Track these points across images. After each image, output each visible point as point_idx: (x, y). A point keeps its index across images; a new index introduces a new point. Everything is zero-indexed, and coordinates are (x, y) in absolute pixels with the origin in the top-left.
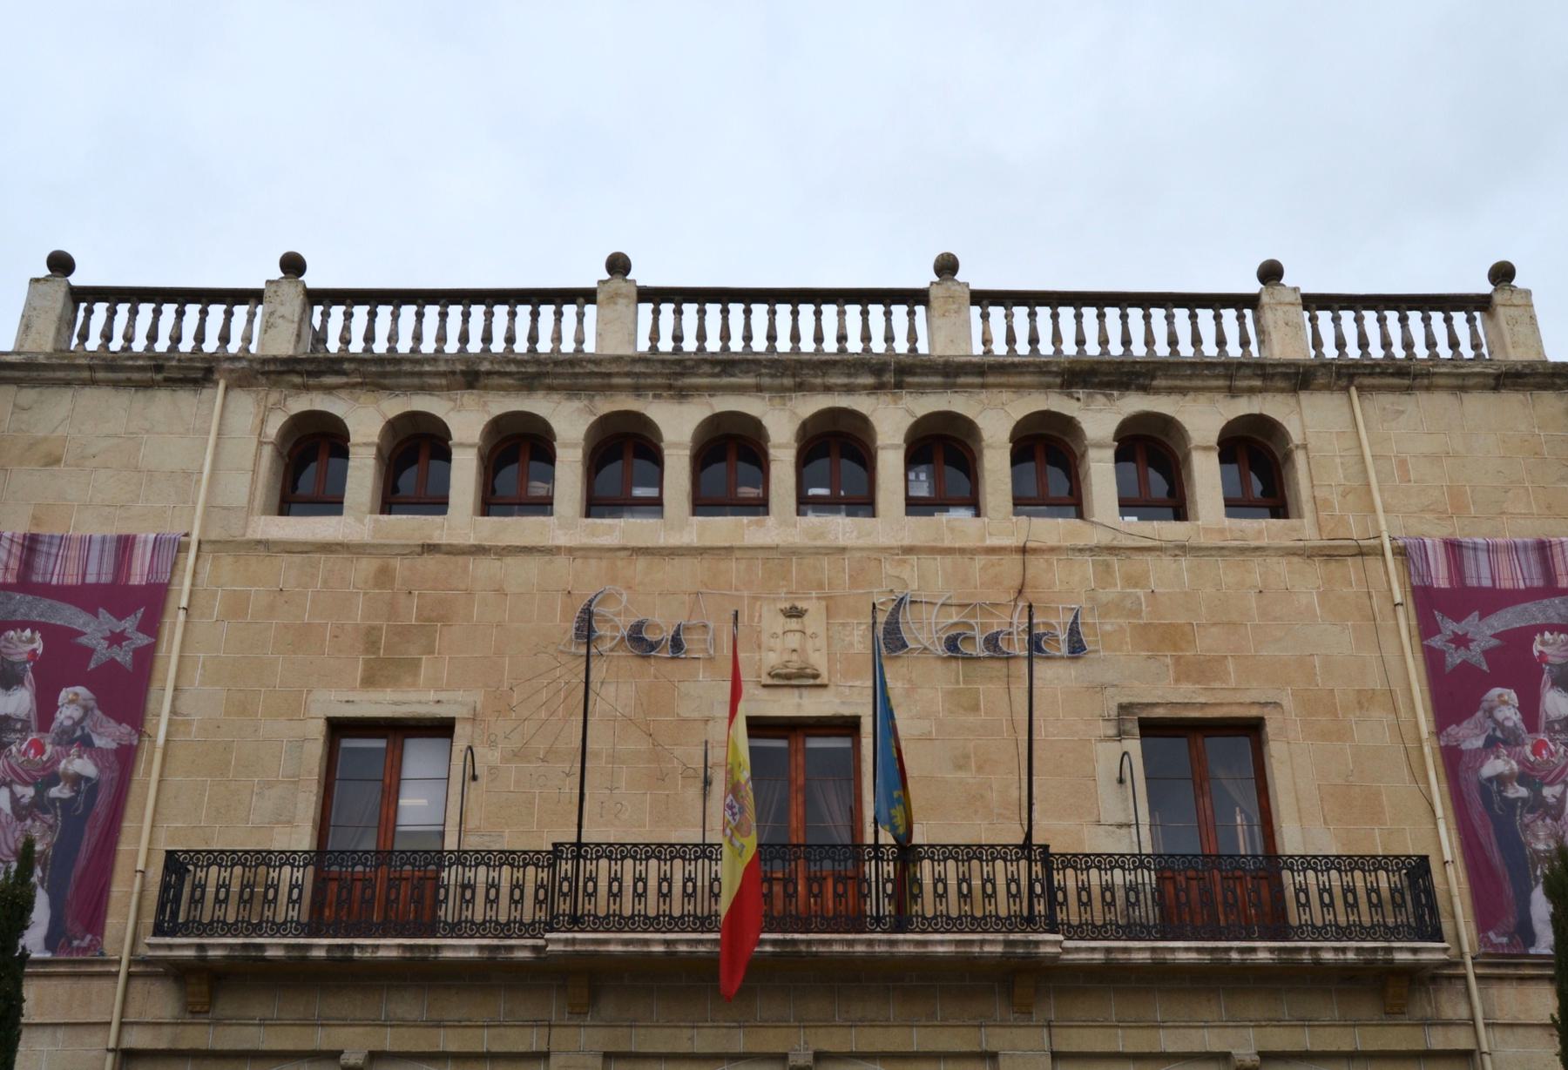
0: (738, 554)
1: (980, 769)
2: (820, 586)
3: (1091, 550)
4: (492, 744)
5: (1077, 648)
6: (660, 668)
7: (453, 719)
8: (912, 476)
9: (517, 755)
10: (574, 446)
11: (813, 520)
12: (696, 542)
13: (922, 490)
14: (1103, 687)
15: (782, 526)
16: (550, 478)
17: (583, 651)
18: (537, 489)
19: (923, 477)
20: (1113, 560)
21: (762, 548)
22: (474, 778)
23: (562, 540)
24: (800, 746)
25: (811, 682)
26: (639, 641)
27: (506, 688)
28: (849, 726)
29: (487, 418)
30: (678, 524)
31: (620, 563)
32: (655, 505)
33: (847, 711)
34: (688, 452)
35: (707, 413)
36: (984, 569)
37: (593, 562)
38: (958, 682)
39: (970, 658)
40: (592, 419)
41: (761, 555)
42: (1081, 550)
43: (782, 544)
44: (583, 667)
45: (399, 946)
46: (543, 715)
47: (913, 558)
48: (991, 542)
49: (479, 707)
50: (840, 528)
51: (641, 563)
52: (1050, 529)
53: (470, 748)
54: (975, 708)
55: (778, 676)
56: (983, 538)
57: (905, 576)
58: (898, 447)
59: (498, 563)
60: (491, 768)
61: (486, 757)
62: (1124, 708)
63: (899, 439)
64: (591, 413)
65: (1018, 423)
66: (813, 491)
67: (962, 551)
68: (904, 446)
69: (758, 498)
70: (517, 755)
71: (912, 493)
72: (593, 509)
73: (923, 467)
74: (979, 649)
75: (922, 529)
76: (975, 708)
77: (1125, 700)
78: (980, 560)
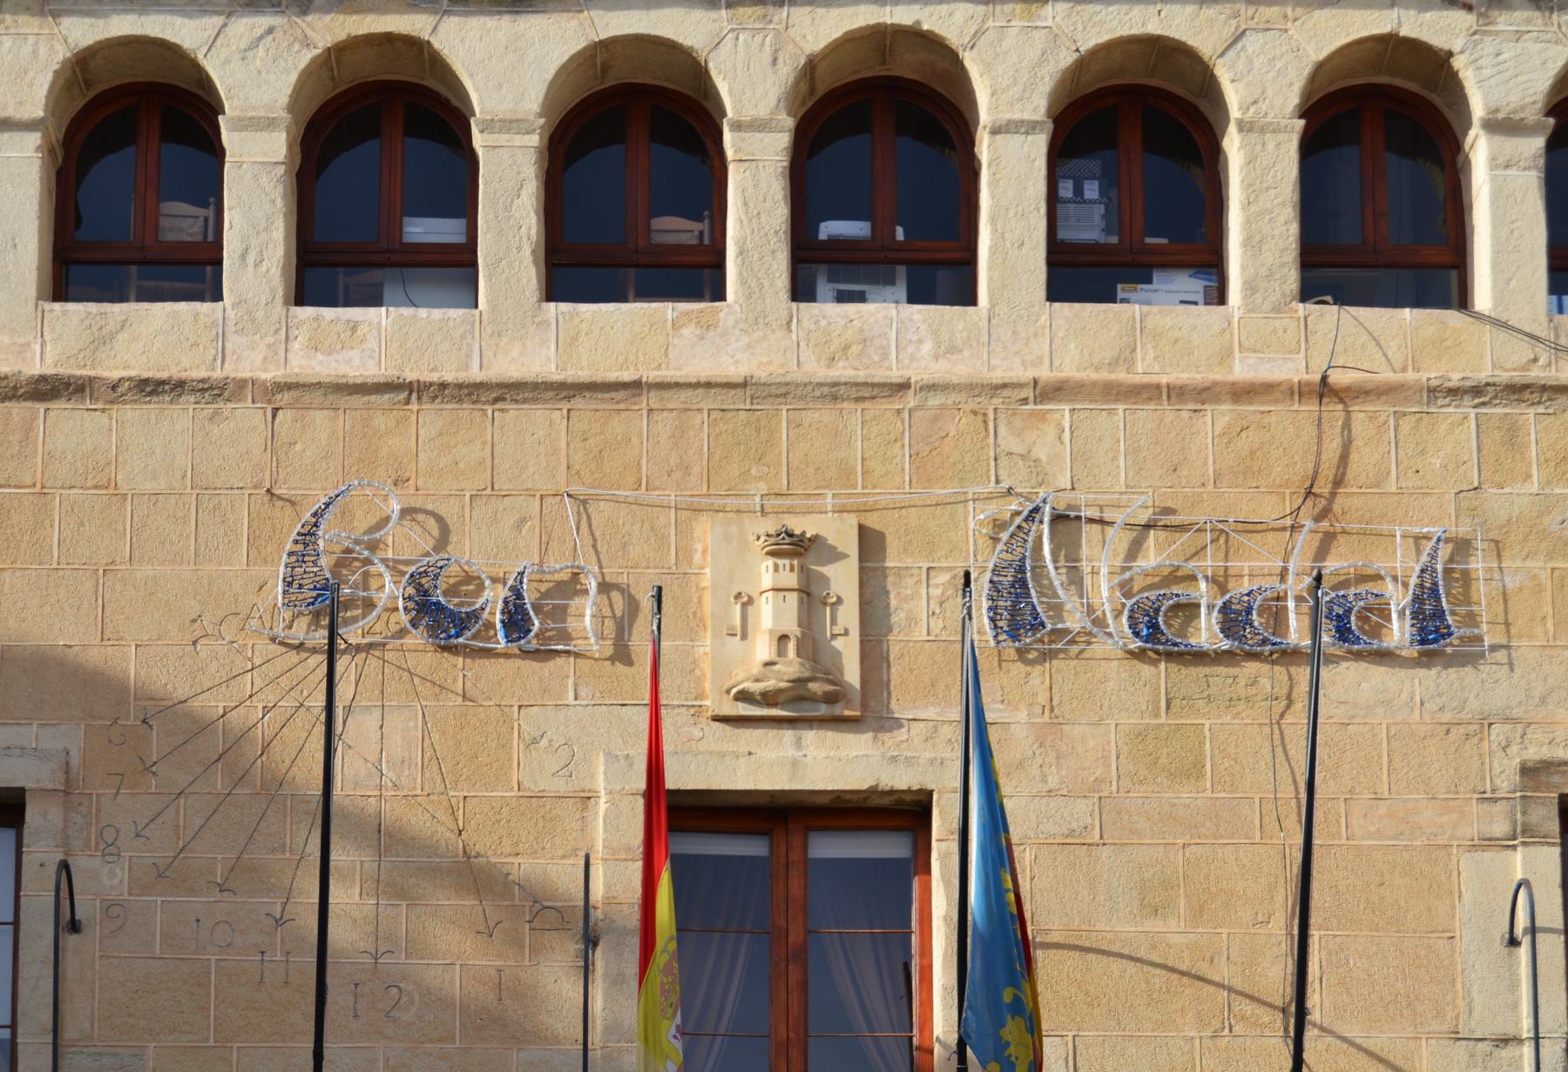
0: (654, 398)
1: (1198, 913)
2: (846, 476)
3: (1477, 391)
4: (110, 850)
5: (1435, 633)
6: (505, 676)
7: (21, 792)
8: (1066, 189)
9: (166, 876)
10: (269, 124)
11: (827, 313)
12: (553, 374)
13: (1089, 228)
14: (1486, 723)
15: (753, 323)
16: (209, 191)
17: (321, 637)
18: (179, 221)
19: (1092, 190)
20: (1529, 415)
21: (709, 385)
22: (75, 927)
23: (251, 361)
24: (795, 856)
25: (823, 710)
26: (441, 617)
27: (132, 720)
28: (909, 814)
29: (61, 54)
30: (509, 319)
31: (381, 421)
32: (455, 267)
33: (902, 779)
34: (534, 140)
35: (576, 44)
36: (1229, 436)
37: (319, 417)
38: (1157, 715)
39: (1200, 657)
40: (306, 57)
41: (708, 401)
42: (1454, 392)
43: (761, 374)
44: (324, 668)
45: (1435, 584)
46: (219, 784)
47: (1063, 412)
48: (1242, 370)
49: (75, 761)
50: (889, 330)
51: (430, 418)
52: (1381, 338)
53: (65, 866)
54: (1195, 771)
55: (744, 696)
56: (1226, 356)
57: (1041, 453)
58: (1031, 127)
59: (103, 419)
60: (108, 907)
61: (101, 881)
62: (1531, 772)
63: (1037, 106)
64: (307, 43)
65: (1320, 66)
66: (831, 229)
67: (1177, 393)
68: (1050, 126)
69: (699, 248)
70: (166, 876)
71: (1063, 234)
72: (918, 803)
73: (1093, 164)
74: (1206, 632)
75: (1087, 335)
76: (1195, 771)
77: (1534, 753)
78: (1222, 415)
